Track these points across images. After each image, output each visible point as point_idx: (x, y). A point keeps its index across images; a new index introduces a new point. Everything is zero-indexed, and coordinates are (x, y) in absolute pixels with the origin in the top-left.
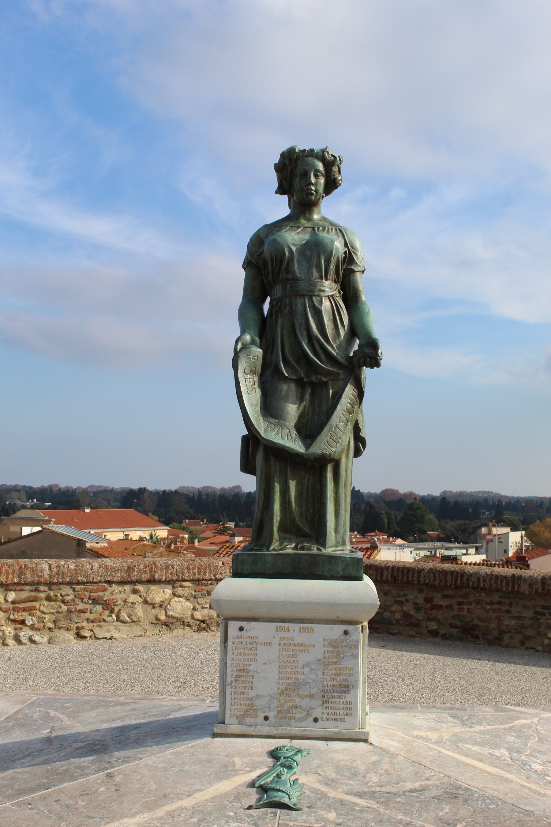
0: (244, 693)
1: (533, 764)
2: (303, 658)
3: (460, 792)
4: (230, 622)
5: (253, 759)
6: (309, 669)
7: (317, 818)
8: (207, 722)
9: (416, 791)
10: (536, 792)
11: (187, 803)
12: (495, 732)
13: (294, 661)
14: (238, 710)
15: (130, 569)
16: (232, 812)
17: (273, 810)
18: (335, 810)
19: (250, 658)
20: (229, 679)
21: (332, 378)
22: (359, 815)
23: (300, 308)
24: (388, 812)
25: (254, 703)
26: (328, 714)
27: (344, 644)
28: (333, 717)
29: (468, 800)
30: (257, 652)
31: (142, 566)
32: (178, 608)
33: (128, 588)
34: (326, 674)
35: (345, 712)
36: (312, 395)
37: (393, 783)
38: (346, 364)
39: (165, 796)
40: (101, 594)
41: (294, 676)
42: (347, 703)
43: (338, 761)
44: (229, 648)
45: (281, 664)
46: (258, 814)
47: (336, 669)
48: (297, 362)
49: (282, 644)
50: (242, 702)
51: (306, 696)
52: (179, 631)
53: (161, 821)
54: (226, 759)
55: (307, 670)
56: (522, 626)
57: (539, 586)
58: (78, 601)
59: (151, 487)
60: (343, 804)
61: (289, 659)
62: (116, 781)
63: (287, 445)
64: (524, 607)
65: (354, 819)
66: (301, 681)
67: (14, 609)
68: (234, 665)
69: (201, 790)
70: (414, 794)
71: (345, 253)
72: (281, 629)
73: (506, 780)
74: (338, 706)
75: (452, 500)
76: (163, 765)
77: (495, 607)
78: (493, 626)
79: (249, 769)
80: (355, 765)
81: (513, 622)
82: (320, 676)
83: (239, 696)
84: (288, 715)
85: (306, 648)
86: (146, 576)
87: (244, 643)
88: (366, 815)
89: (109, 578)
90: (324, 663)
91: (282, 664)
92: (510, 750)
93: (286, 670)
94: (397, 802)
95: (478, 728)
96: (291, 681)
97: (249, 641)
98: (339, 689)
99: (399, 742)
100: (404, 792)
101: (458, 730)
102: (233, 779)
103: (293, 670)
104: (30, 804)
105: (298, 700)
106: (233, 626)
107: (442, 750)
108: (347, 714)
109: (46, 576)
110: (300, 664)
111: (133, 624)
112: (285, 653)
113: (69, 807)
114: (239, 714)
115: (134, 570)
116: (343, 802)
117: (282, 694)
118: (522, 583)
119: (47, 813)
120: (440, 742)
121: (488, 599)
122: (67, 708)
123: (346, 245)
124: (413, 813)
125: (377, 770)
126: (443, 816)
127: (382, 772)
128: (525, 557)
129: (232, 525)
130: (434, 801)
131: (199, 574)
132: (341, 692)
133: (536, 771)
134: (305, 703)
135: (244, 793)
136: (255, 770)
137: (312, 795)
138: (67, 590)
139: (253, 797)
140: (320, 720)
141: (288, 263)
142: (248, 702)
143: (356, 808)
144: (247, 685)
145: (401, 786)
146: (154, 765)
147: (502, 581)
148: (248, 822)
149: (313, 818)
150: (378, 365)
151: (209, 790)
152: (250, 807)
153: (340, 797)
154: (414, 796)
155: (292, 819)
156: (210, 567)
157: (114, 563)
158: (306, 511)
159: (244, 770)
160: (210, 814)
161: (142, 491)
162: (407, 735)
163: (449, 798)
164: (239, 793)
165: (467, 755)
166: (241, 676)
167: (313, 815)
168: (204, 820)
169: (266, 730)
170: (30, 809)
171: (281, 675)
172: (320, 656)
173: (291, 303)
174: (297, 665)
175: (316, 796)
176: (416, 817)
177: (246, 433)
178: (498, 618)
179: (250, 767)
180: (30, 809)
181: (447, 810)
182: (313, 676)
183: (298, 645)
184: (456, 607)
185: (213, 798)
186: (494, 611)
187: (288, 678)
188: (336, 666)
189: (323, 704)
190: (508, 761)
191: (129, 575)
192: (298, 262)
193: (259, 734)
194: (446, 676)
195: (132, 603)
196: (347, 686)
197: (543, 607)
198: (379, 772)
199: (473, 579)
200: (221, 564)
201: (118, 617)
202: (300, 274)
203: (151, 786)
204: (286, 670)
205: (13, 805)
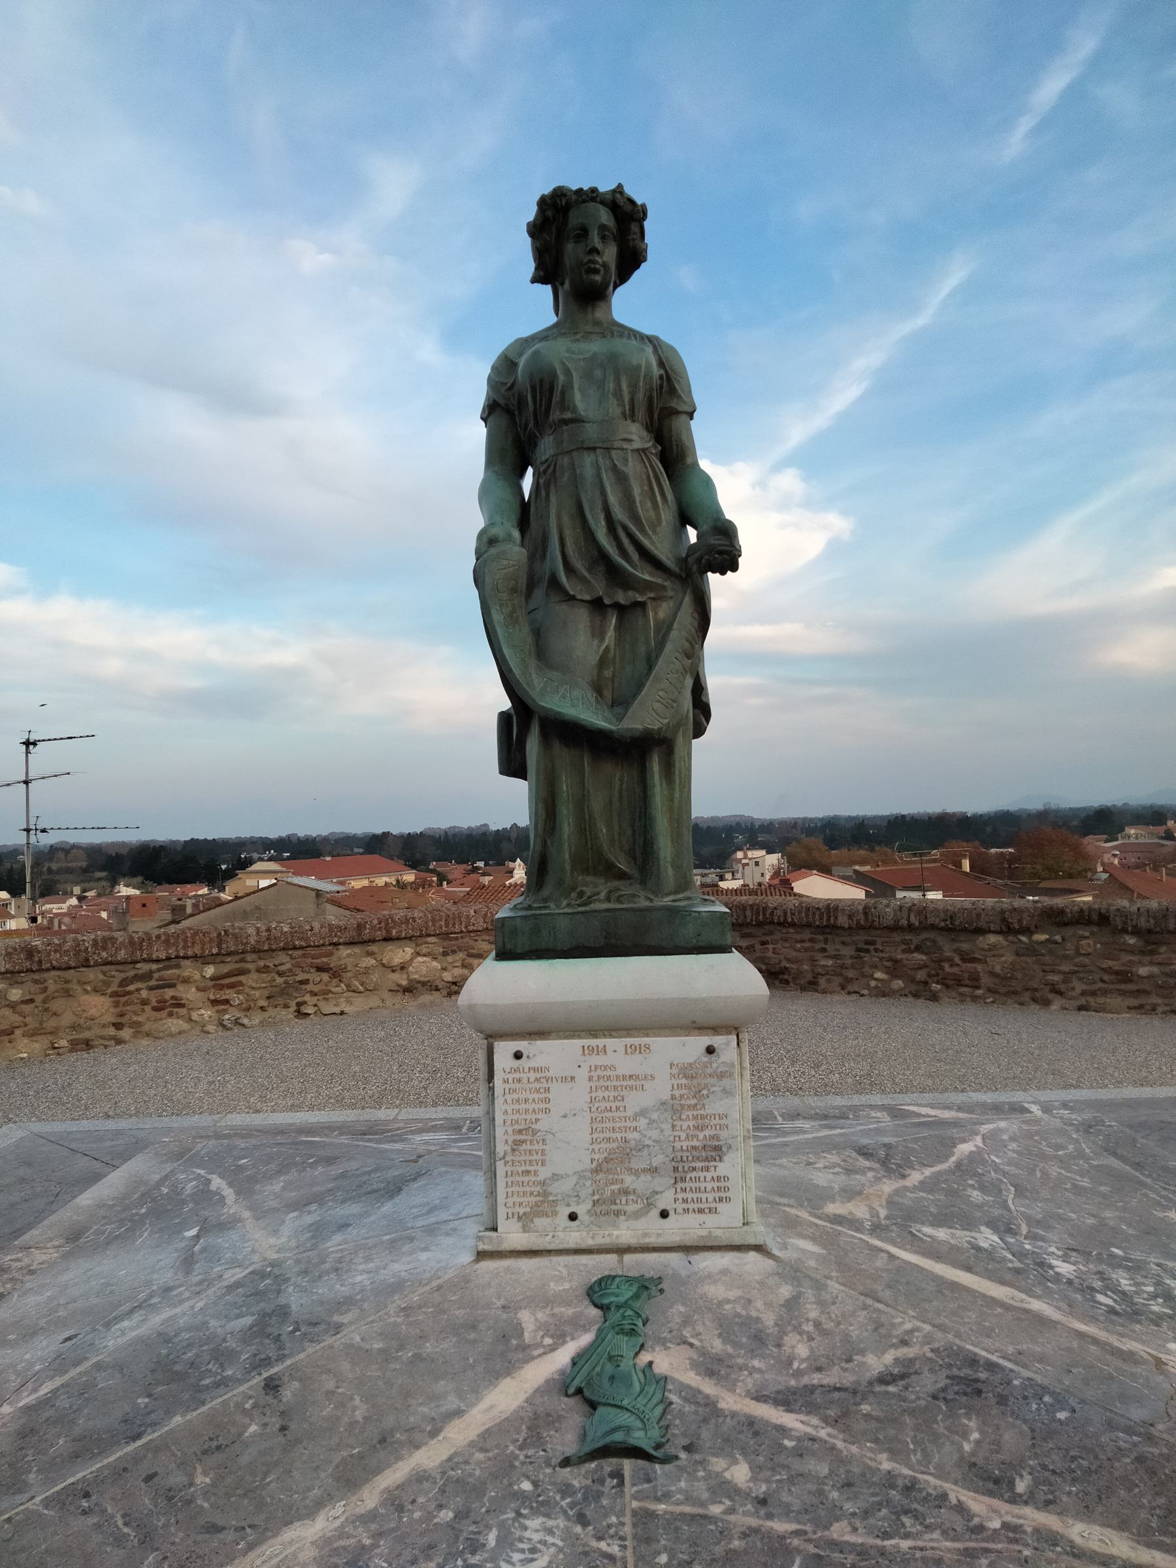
0: (528, 1172)
2: (635, 1101)
4: (496, 1044)
5: (556, 1310)
8: (464, 1214)
11: (429, 1457)
14: (521, 1204)
15: (360, 927)
16: (528, 1478)
19: (536, 1107)
20: (501, 1148)
21: (652, 595)
22: (797, 1465)
23: (588, 472)
24: (854, 1449)
25: (550, 1189)
26: (685, 1201)
27: (708, 1071)
28: (696, 1206)
30: (550, 1096)
31: (375, 922)
32: (424, 969)
33: (357, 950)
35: (717, 1195)
36: (619, 627)
38: (677, 570)
39: (383, 1441)
40: (325, 960)
41: (619, 1136)
43: (720, 1304)
44: (498, 1091)
47: (695, 1117)
48: (590, 570)
49: (595, 1078)
50: (528, 1189)
51: (644, 1170)
52: (426, 998)
53: (373, 1526)
54: (505, 1316)
55: (642, 1123)
56: (842, 967)
57: (861, 917)
58: (298, 971)
59: (395, 831)
61: (608, 1105)
62: (284, 1400)
63: (582, 716)
64: (843, 943)
65: (791, 1480)
66: (633, 1142)
67: (214, 986)
68: (509, 1122)
71: (661, 377)
72: (592, 1050)
73: (1041, 1321)
74: (702, 1185)
75: (704, 826)
76: (381, 1345)
77: (807, 945)
78: (806, 967)
80: (754, 1314)
81: (830, 962)
82: (668, 1132)
83: (521, 1179)
84: (614, 1207)
85: (638, 1083)
87: (525, 1081)
89: (335, 940)
90: (673, 1108)
93: (604, 1125)
96: (615, 1145)
97: (533, 1076)
98: (704, 1154)
99: (813, 1239)
100: (870, 1383)
103: (618, 1125)
104: (87, 1495)
105: (629, 1180)
106: (504, 1051)
108: (721, 1200)
109: (253, 942)
110: (629, 1113)
111: (368, 993)
112: (600, 1094)
114: (522, 1211)
117: (596, 1171)
119: (120, 1523)
121: (799, 937)
122: (241, 1169)
123: (661, 364)
125: (800, 1325)
126: (973, 1453)
127: (808, 1327)
129: (481, 864)
132: (707, 1159)
133: (1070, 1282)
134: (641, 1184)
135: (548, 1415)
136: (564, 1342)
138: (282, 957)
140: (671, 1213)
141: (563, 393)
142: (538, 1188)
144: (535, 1157)
145: (858, 1365)
146: (363, 1344)
147: (814, 914)
149: (702, 1485)
152: (566, 1462)
153: (747, 1410)
154: (893, 1395)
155: (660, 1494)
160: (478, 1490)
161: (386, 835)
164: (536, 1416)
165: (938, 1257)
167: (701, 1474)
169: (574, 1236)
171: (595, 1136)
172: (666, 1096)
173: (573, 467)
175: (696, 1413)
176: (919, 1462)
177: (506, 704)
178: (813, 960)
179: (552, 1337)
182: (654, 1134)
183: (624, 1077)
184: (758, 947)
186: (806, 950)
188: (695, 1113)
189: (676, 1182)
192: (580, 390)
193: (561, 1247)
196: (718, 1148)
197: (867, 943)
198: (805, 1327)
199: (779, 912)
201: (348, 986)
203: (355, 1409)
204: (604, 1125)
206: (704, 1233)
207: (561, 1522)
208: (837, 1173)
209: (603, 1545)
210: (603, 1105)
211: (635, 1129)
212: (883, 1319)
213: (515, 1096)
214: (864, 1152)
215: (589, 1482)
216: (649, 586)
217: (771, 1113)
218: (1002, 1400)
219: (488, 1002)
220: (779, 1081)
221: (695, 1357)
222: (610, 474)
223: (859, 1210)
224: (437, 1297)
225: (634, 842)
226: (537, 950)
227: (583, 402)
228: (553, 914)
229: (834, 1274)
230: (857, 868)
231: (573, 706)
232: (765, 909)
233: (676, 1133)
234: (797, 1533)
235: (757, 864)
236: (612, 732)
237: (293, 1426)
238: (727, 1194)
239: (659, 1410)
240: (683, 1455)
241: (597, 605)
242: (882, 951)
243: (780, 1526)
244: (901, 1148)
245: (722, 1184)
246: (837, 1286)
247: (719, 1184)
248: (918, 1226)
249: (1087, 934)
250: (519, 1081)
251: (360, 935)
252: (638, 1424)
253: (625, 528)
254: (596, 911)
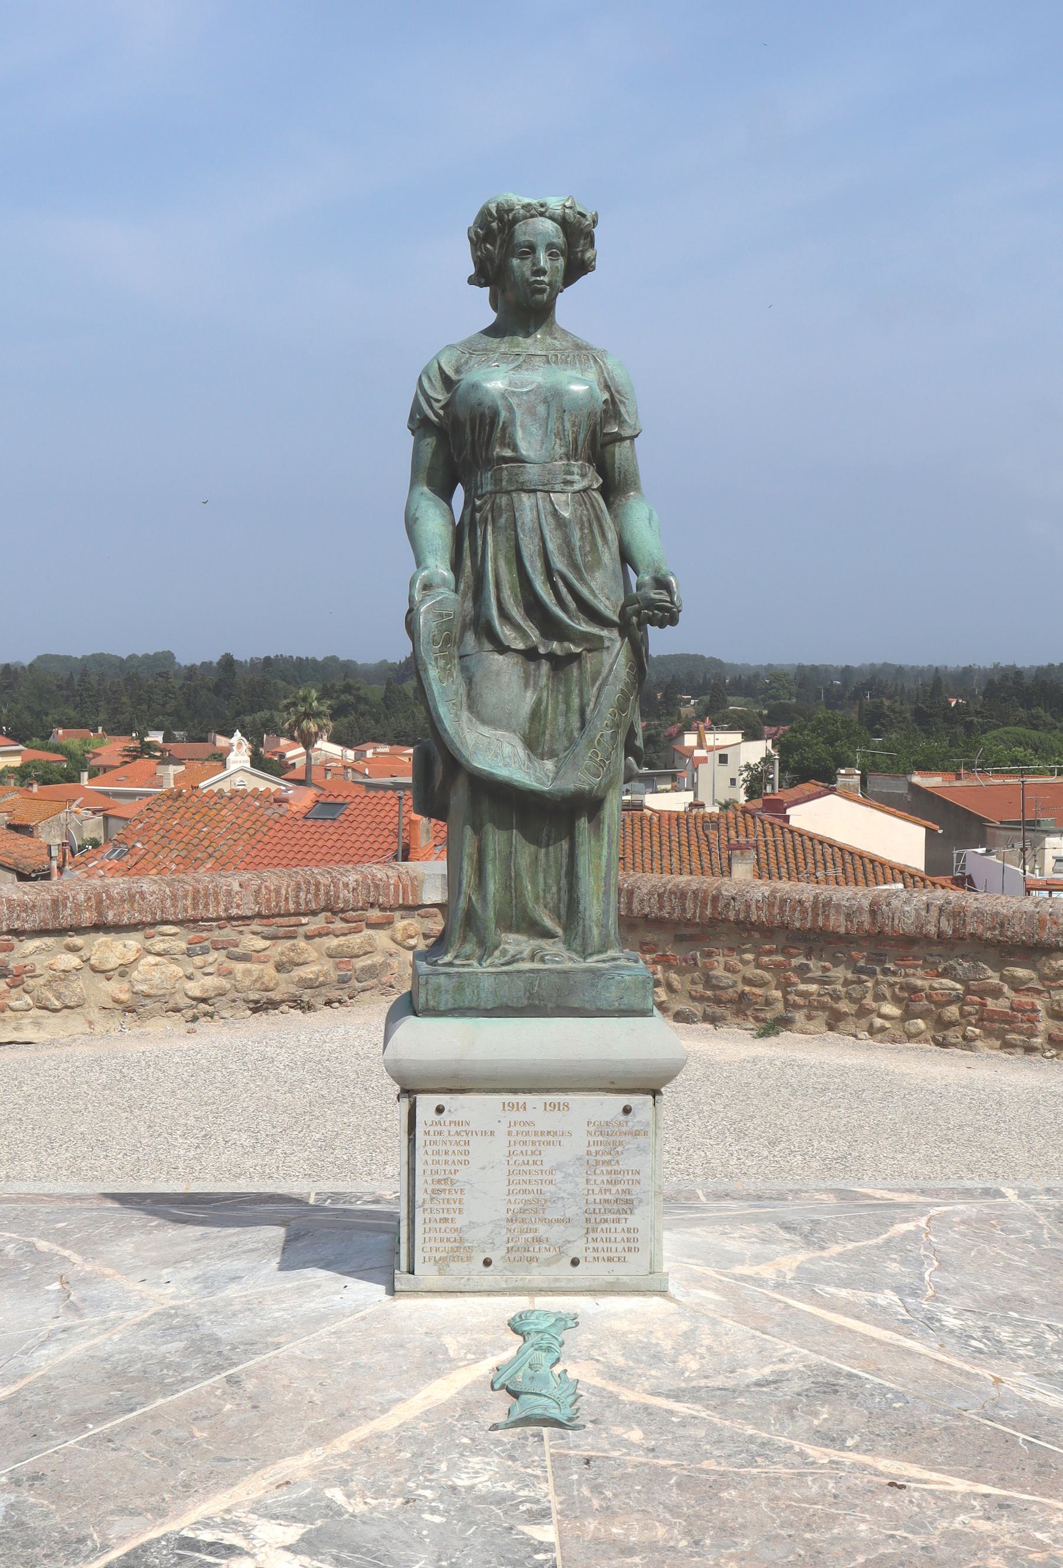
1: (944, 1318)
2: (551, 1156)
3: (842, 1382)
5: (475, 1336)
6: (563, 1175)
7: (612, 1440)
9: (768, 1383)
10: (962, 1373)
11: (386, 1423)
12: (864, 1255)
13: (535, 1163)
14: (437, 1250)
15: (56, 904)
17: (535, 1429)
18: (639, 1423)
19: (456, 1158)
20: (419, 1196)
22: (680, 1432)
24: (727, 1423)
26: (595, 1250)
28: (606, 1255)
29: (857, 1395)
33: (49, 941)
34: (592, 1182)
35: (626, 1245)
37: (726, 1371)
39: (342, 1415)
42: (629, 1231)
43: (624, 1334)
45: (512, 1168)
46: (511, 1439)
47: (609, 1173)
49: (514, 1133)
50: (445, 1235)
51: (558, 1221)
52: (160, 1026)
54: (428, 1339)
57: (866, 918)
60: (651, 1414)
61: (525, 1158)
65: (675, 1439)
69: (400, 1400)
70: (764, 1389)
73: (909, 1352)
79: (473, 1357)
80: (654, 1341)
83: (438, 1226)
84: (527, 1254)
85: (555, 1139)
86: (88, 917)
87: (446, 1133)
88: (692, 1431)
89: (17, 925)
90: (590, 1163)
91: (514, 1167)
92: (898, 1290)
93: (521, 1178)
94: (740, 1405)
95: (835, 1249)
97: (454, 1129)
99: (716, 1290)
100: (748, 1386)
101: (802, 1256)
102: (451, 1376)
104: (110, 1441)
105: (542, 1229)
106: (426, 1104)
107: (791, 1302)
108: (630, 1250)
110: (546, 1167)
112: (519, 1148)
113: (180, 1444)
114: (438, 1255)
115: (65, 906)
116: (650, 1410)
117: (510, 1221)
118: (833, 911)
120: (782, 1285)
124: (770, 1424)
125: (695, 1348)
126: (820, 1426)
127: (703, 1350)
128: (780, 801)
129: (156, 737)
130: (801, 1401)
131: (194, 909)
133: (952, 1331)
136: (485, 1358)
137: (594, 1399)
139: (500, 1407)
142: (455, 1235)
143: (673, 1419)
144: (452, 1206)
148: (498, 1454)
150: (673, 620)
151: (414, 1399)
152: (495, 1427)
153: (643, 1401)
154: (766, 1393)
156: (216, 894)
157: (25, 893)
158: (544, 891)
159: (465, 1359)
160: (429, 1442)
162: (725, 1276)
163: (825, 1392)
164: (468, 1403)
165: (833, 1309)
166: (440, 1191)
168: (422, 1454)
170: (114, 1450)
171: (512, 1187)
174: (541, 1168)
175: (601, 1402)
179: (474, 1353)
180: (114, 1450)
181: (826, 1416)
183: (542, 1133)
185: (425, 1413)
187: (525, 1192)
188: (609, 1169)
190: (902, 1315)
191: (55, 917)
194: (699, 1103)
195: (64, 971)
198: (698, 1350)
200: (236, 887)
202: (527, 450)
204: (521, 1178)
205: (81, 1443)
206: (611, 1279)
207: (496, 1459)
208: (753, 1243)
209: (529, 1471)
210: (521, 1158)
211: (551, 1182)
212: (768, 1345)
213: (435, 1148)
214: (787, 1227)
215: (516, 1439)
216: (586, 637)
217: (693, 1192)
218: (853, 1396)
219: (413, 1058)
220: (715, 1163)
221: (601, 1368)
222: (550, 519)
223: (767, 1272)
224: (363, 1325)
225: (559, 900)
226: (460, 1008)
227: (529, 441)
228: (477, 974)
229: (731, 1314)
230: (916, 779)
231: (505, 766)
232: (715, 899)
233: (589, 1187)
234: (675, 1465)
235: (723, 759)
236: (543, 792)
237: (262, 1406)
238: (636, 1235)
239: (571, 1399)
240: (590, 1425)
241: (530, 655)
242: (894, 973)
243: (662, 1462)
244: (830, 1224)
245: (632, 1235)
246: (731, 1322)
247: (629, 1235)
248: (822, 1286)
250: (440, 1133)
251: (55, 917)
252: (554, 1404)
253: (564, 578)
254: (519, 972)
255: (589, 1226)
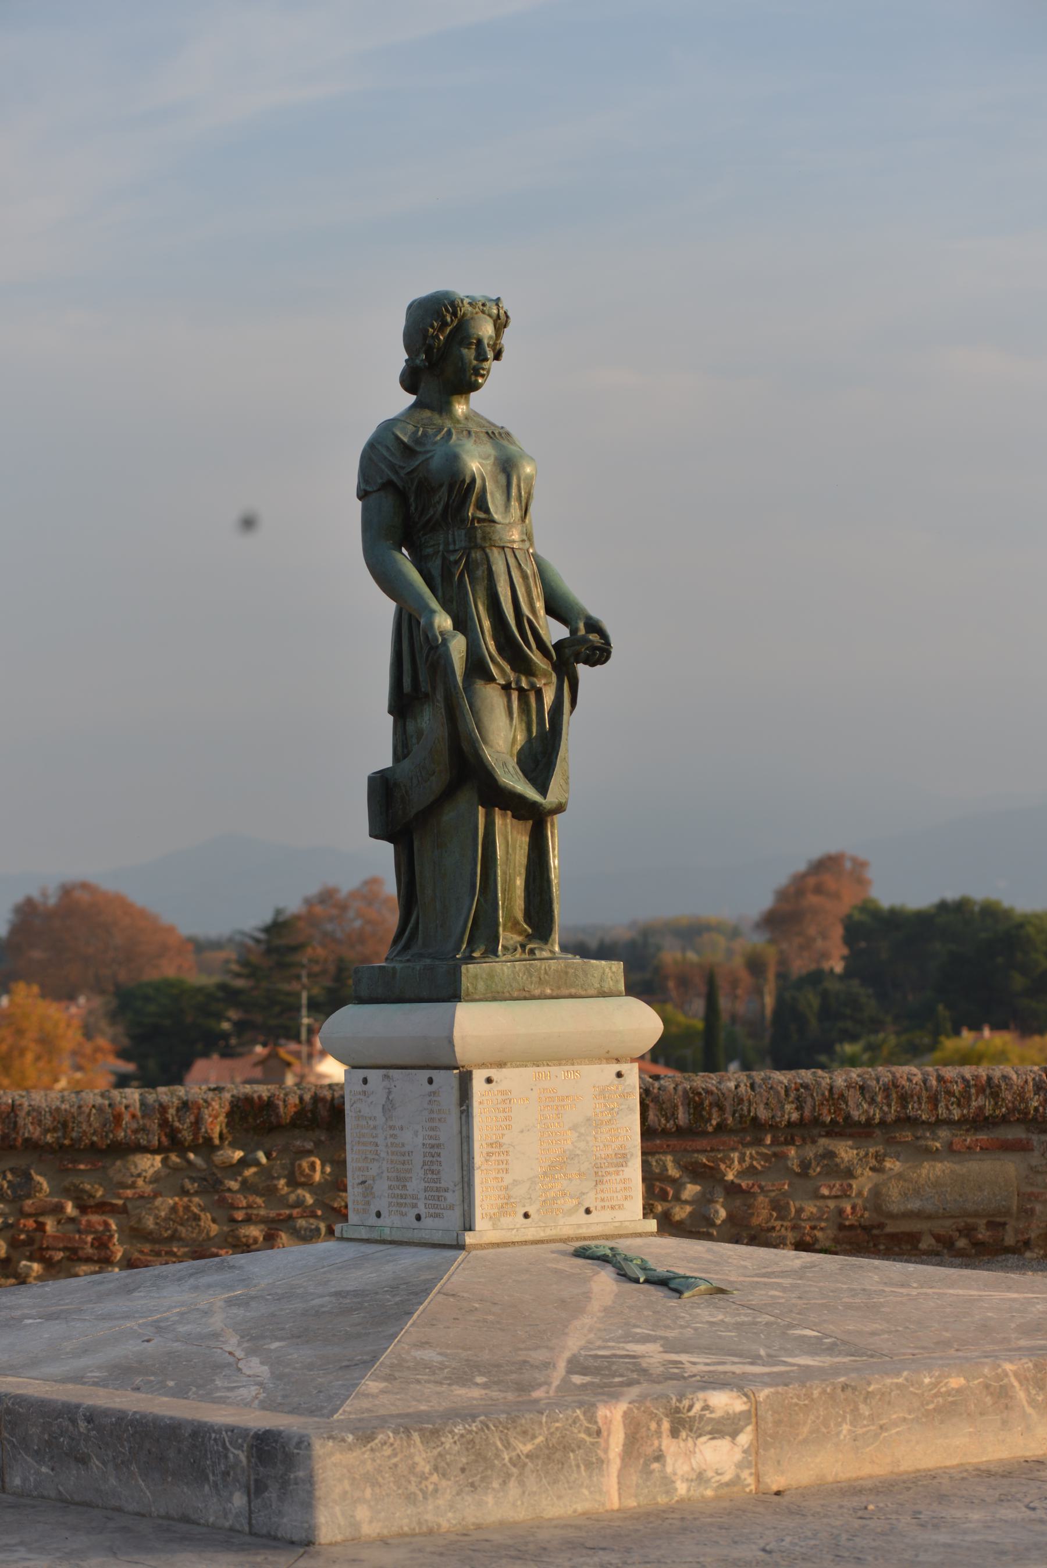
26: (603, 1200)
30: (441, 1159)
196: (624, 1156)
236: (541, 805)
241: (506, 688)
249: (309, 1146)
255: (598, 1179)
